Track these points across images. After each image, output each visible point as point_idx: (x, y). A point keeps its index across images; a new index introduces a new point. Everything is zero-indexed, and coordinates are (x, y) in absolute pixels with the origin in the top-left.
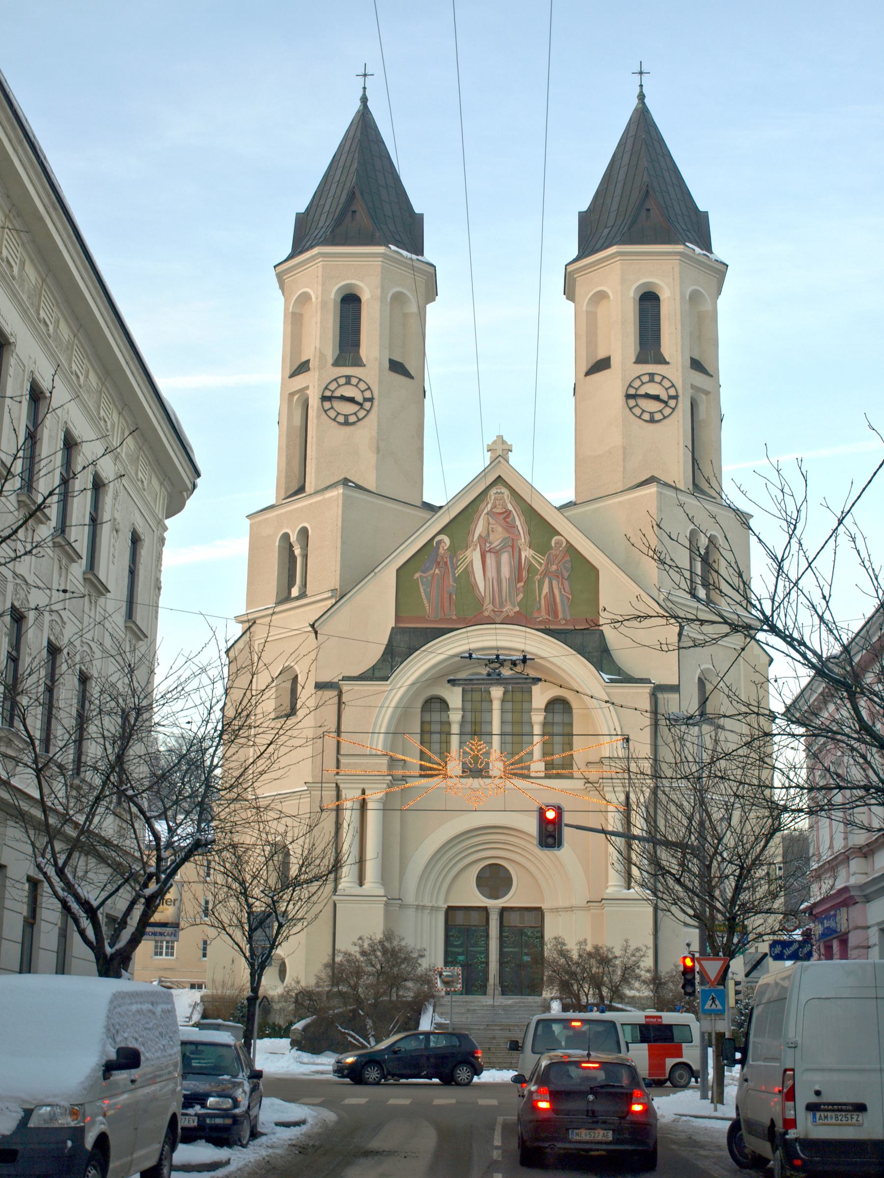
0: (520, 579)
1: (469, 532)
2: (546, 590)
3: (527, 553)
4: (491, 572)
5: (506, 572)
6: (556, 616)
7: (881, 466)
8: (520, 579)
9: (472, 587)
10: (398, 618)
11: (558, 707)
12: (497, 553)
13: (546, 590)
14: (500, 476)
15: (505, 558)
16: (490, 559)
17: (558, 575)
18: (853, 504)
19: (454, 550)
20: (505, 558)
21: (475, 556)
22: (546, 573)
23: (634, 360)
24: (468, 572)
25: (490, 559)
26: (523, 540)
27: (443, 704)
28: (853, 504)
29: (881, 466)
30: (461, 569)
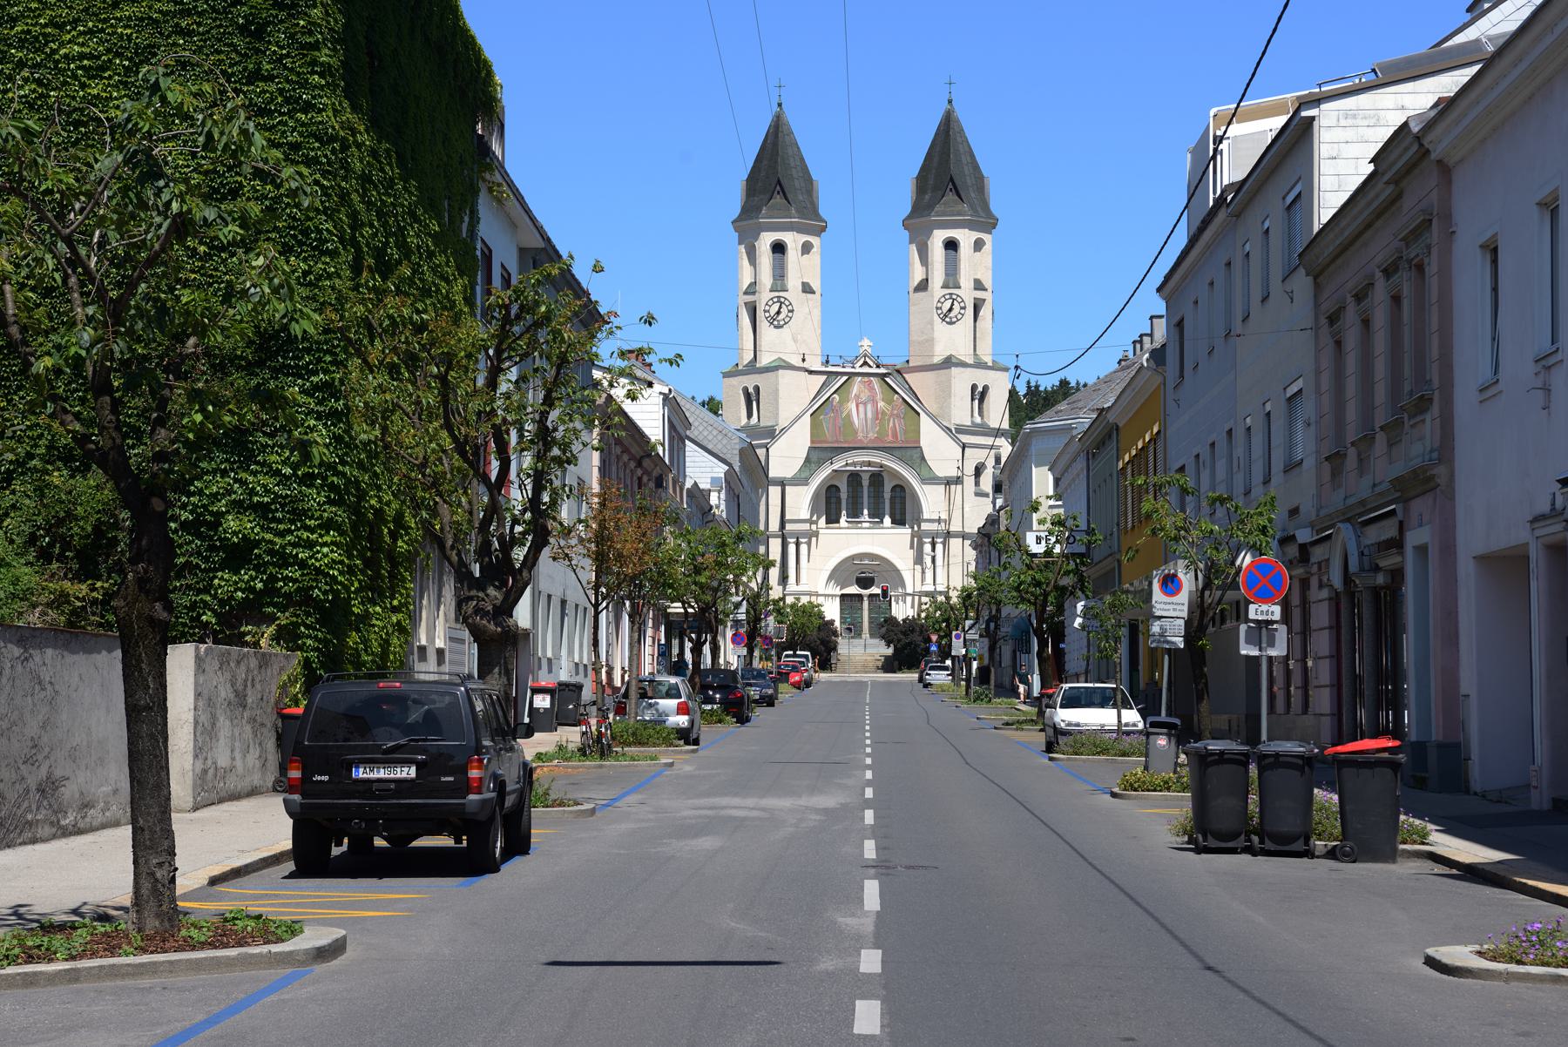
0: (877, 419)
1: (849, 392)
2: (891, 424)
3: (881, 404)
4: (862, 415)
5: (869, 415)
6: (897, 438)
7: (1320, 1040)
8: (877, 419)
9: (851, 423)
10: (812, 442)
11: (898, 489)
12: (865, 404)
13: (891, 424)
14: (975, 289)
15: (869, 407)
16: (861, 408)
17: (898, 416)
18: (1178, 220)
19: (842, 402)
20: (869, 407)
21: (853, 406)
22: (892, 415)
23: (1316, 123)
24: (849, 415)
25: (861, 408)
26: (879, 396)
27: (837, 489)
28: (1178, 220)
29: (1320, 1040)
30: (844, 415)
